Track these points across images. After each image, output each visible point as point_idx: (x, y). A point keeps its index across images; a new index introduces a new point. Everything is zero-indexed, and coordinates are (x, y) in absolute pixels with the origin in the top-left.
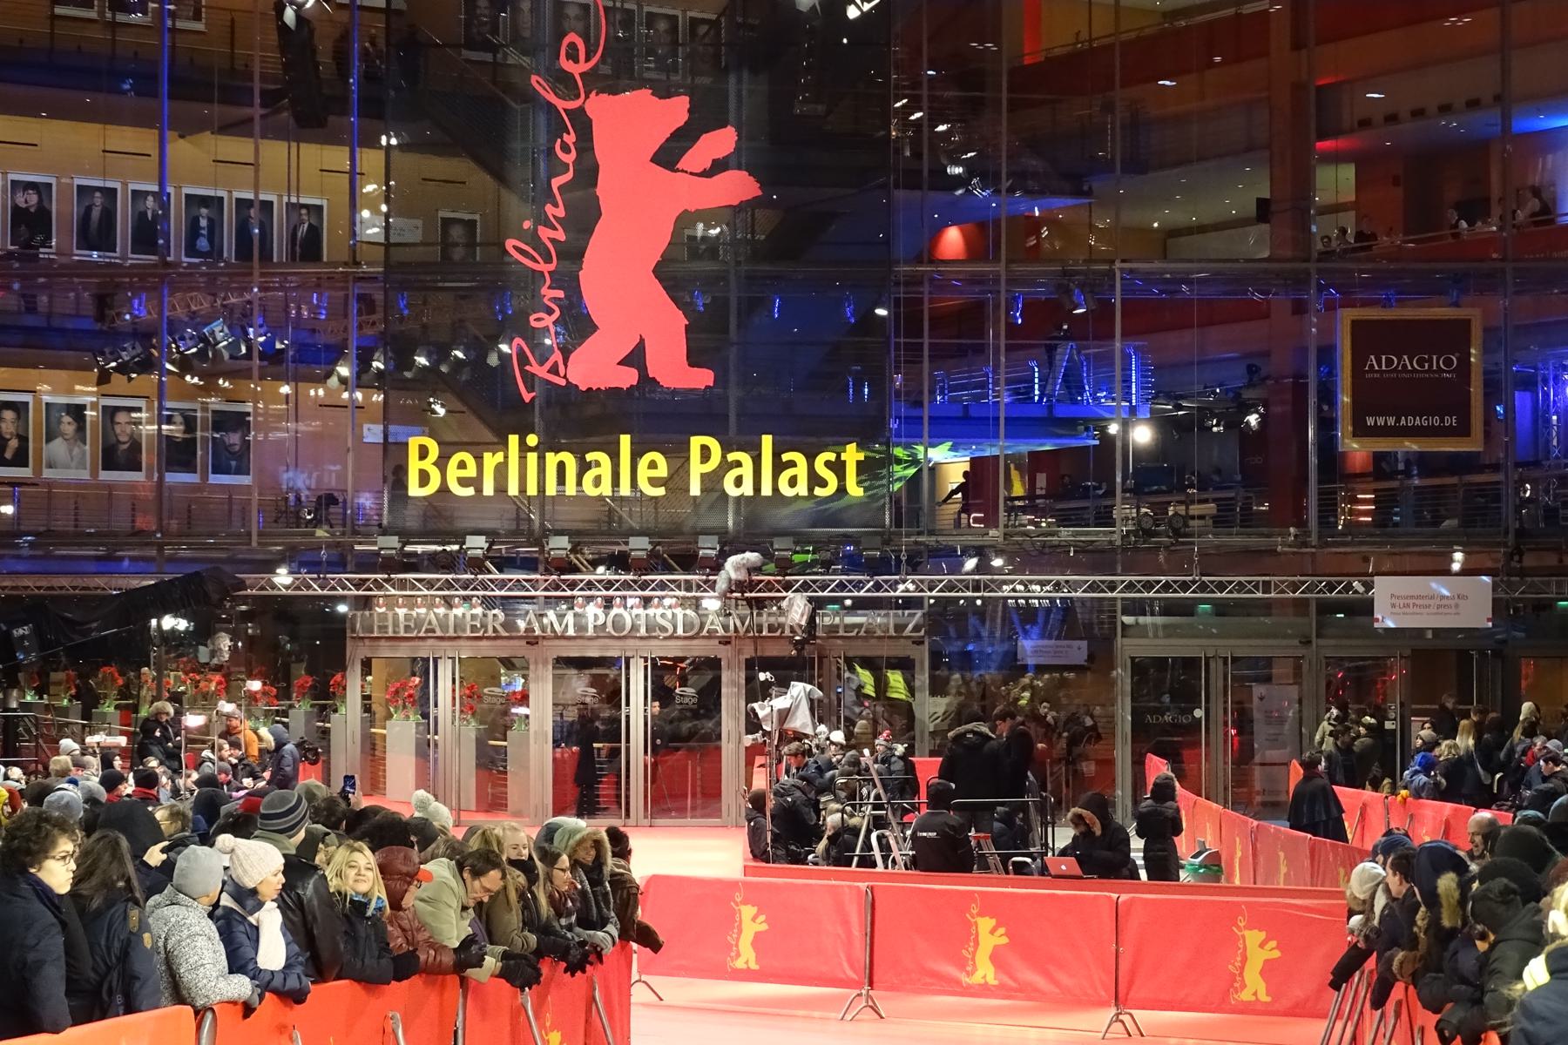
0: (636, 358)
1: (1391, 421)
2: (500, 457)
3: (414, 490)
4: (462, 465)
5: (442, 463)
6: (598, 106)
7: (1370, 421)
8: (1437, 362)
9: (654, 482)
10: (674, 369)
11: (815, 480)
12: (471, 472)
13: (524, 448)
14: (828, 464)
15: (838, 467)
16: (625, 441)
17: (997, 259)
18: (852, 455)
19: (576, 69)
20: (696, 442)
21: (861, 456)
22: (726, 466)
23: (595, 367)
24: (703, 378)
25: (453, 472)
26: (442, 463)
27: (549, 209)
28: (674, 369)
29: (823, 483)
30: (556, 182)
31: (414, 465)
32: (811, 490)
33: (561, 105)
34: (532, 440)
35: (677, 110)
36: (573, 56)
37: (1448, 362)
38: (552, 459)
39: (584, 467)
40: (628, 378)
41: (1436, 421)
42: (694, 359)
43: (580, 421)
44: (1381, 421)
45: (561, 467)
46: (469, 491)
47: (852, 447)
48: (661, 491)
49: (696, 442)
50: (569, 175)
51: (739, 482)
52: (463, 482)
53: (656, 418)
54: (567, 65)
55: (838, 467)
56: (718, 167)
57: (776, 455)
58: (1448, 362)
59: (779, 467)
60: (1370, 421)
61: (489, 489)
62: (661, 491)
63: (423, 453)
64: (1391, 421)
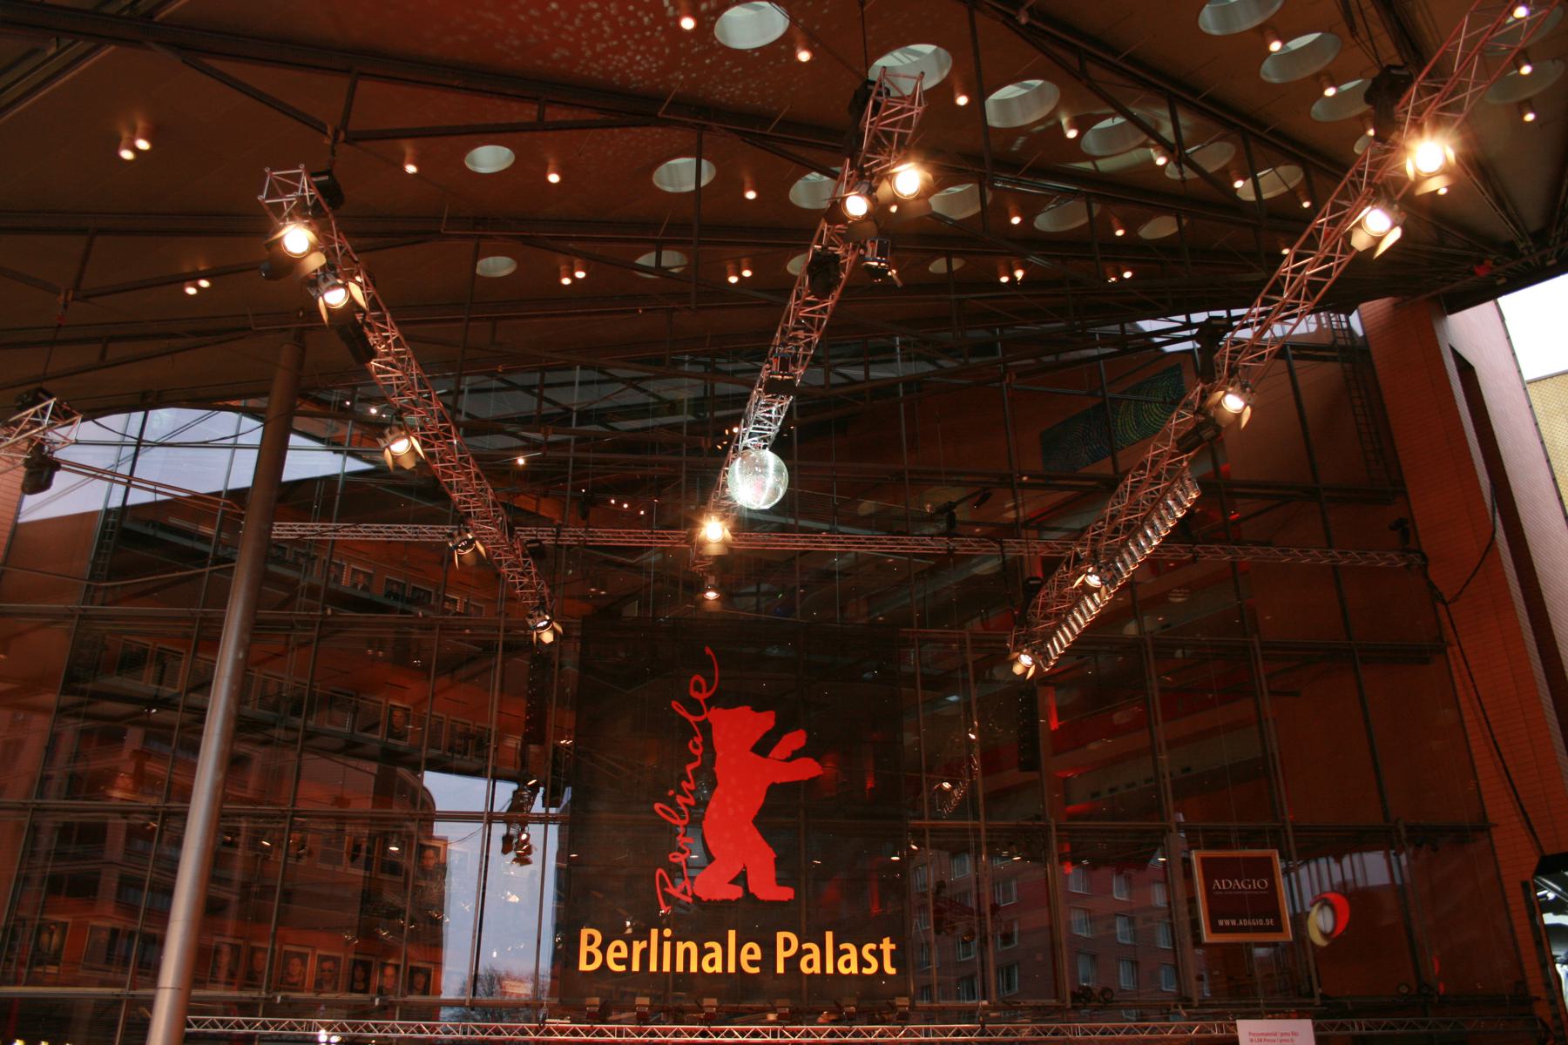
0: (741, 879)
1: (1234, 922)
2: (644, 944)
3: (583, 966)
4: (617, 950)
5: (603, 948)
6: (715, 715)
7: (1221, 923)
8: (1256, 884)
9: (752, 963)
10: (767, 887)
11: (863, 963)
12: (624, 954)
13: (661, 939)
14: (871, 952)
15: (878, 954)
16: (732, 934)
17: (976, 817)
18: (887, 946)
19: (701, 697)
20: (781, 936)
21: (893, 946)
22: (801, 953)
23: (715, 885)
24: (786, 894)
25: (611, 955)
26: (603, 948)
27: (684, 784)
28: (767, 887)
29: (869, 965)
30: (690, 768)
31: (584, 949)
32: (860, 968)
33: (692, 719)
34: (667, 933)
35: (767, 720)
36: (698, 688)
37: (1262, 884)
38: (681, 947)
39: (702, 952)
40: (736, 892)
41: (1261, 922)
42: (781, 882)
43: (704, 922)
44: (1227, 922)
45: (687, 952)
46: (622, 968)
47: (887, 940)
48: (756, 970)
49: (781, 936)
50: (698, 763)
51: (810, 964)
52: (618, 961)
53: (757, 922)
54: (695, 695)
55: (878, 954)
56: (795, 755)
57: (836, 946)
58: (1262, 884)
59: (838, 954)
60: (1221, 923)
61: (636, 967)
62: (756, 970)
63: (591, 940)
64: (1234, 922)
